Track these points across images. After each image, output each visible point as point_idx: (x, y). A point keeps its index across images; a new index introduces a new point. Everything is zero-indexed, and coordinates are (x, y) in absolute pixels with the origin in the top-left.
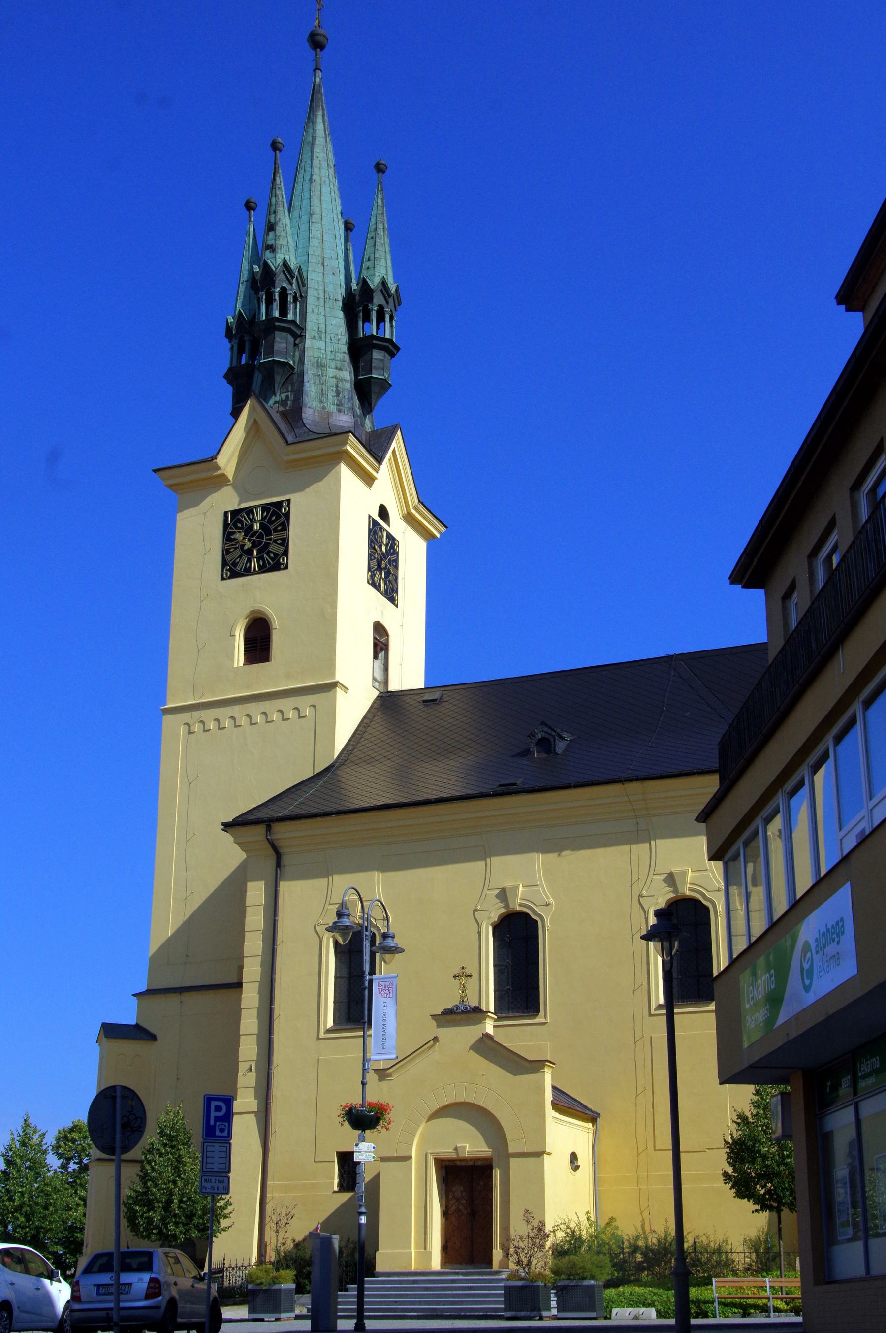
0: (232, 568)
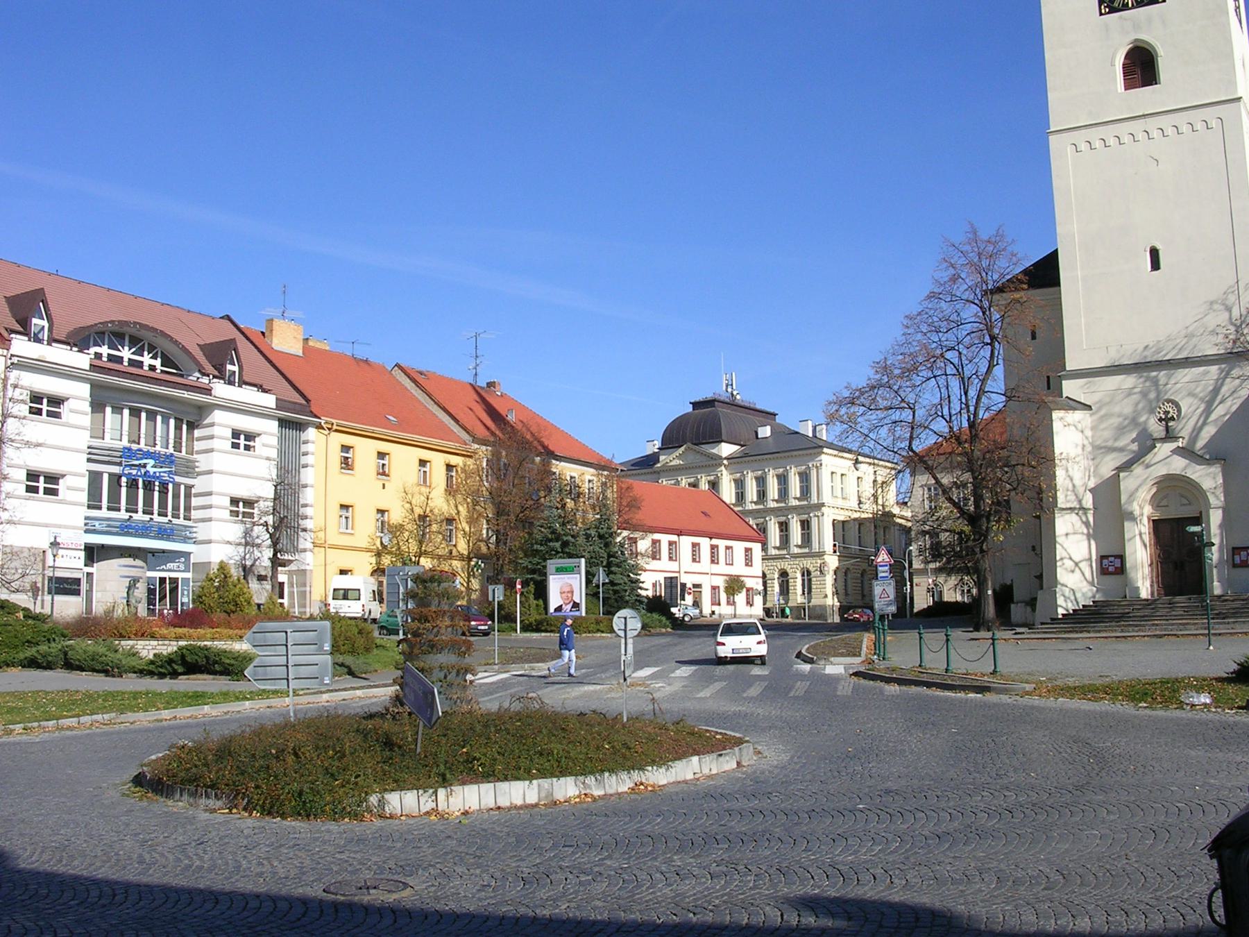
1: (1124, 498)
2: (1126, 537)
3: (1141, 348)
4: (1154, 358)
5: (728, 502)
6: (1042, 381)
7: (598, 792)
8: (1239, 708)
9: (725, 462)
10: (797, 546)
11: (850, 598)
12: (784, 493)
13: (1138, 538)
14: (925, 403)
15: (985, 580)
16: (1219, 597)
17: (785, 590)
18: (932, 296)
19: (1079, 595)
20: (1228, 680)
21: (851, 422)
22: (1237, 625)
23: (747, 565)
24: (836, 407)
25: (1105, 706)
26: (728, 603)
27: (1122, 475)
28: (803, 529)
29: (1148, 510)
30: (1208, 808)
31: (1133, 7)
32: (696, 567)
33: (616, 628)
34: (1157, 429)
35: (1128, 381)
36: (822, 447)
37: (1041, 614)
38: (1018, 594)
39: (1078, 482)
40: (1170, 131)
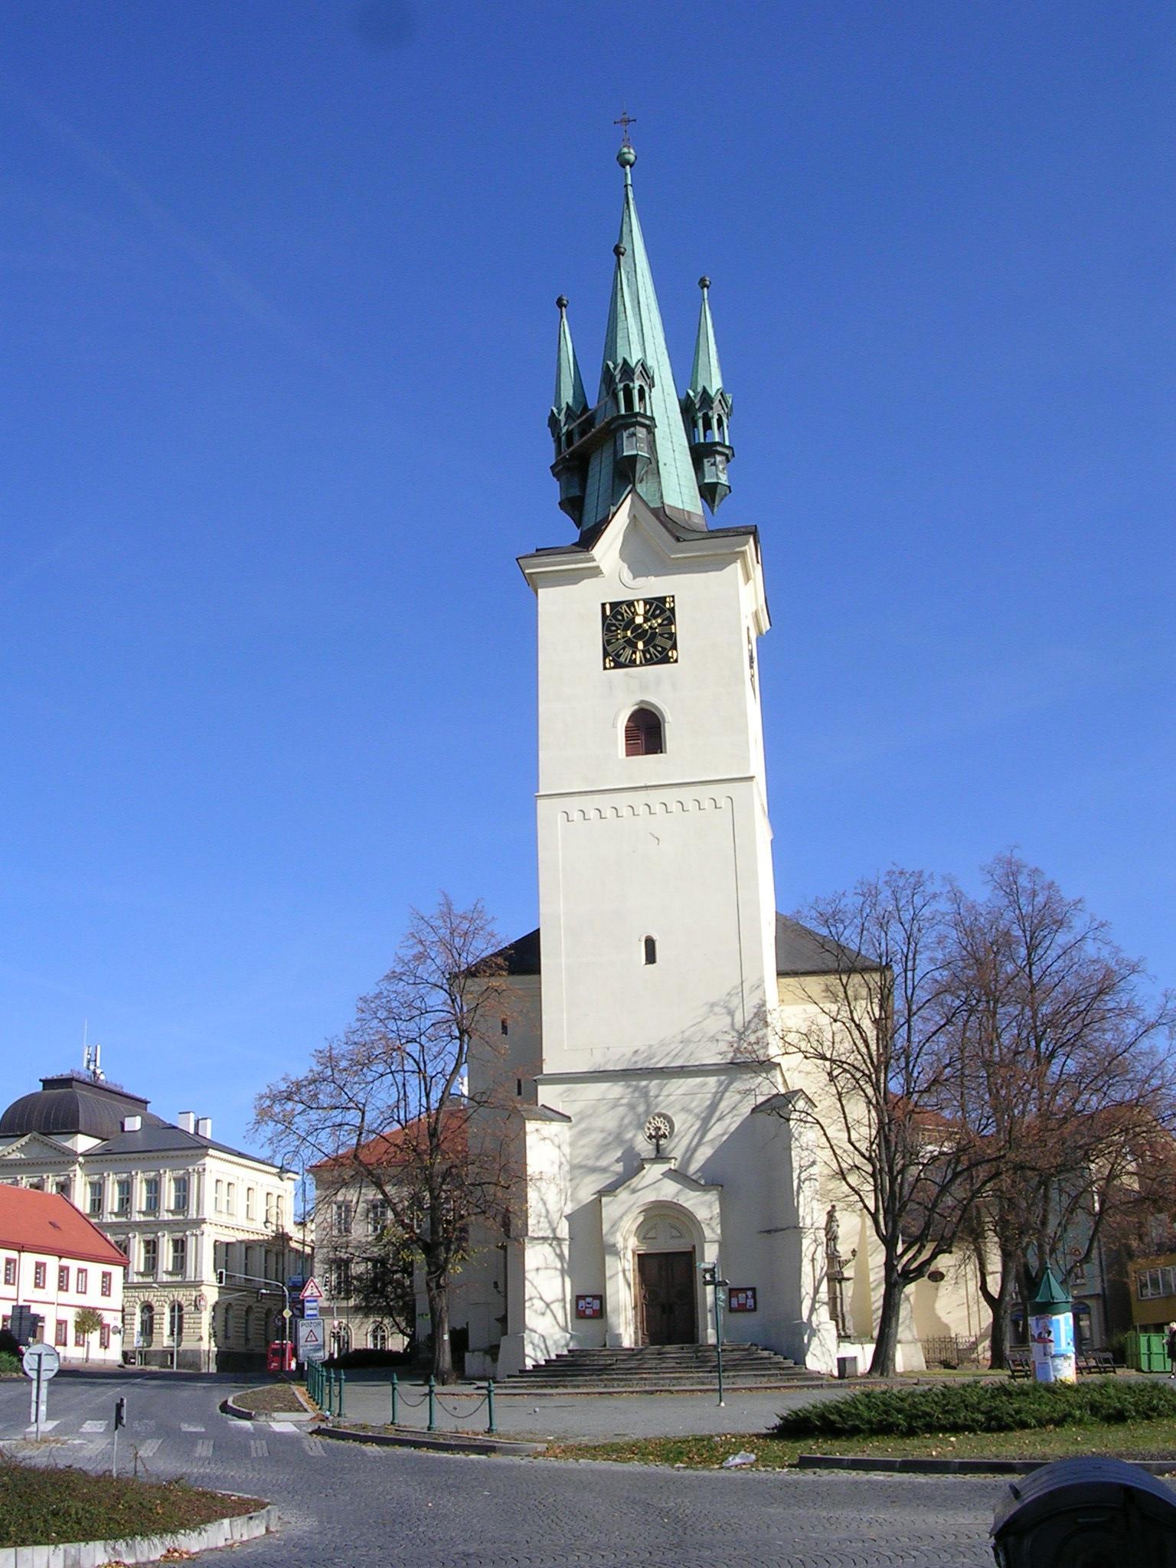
0: (615, 656)
1: (605, 1228)
2: (608, 1274)
3: (629, 1054)
4: (645, 1066)
5: (81, 1209)
6: (515, 1082)
7: (129, 1560)
8: (791, 1466)
9: (81, 1159)
10: (138, 1273)
11: (231, 1342)
12: (154, 1203)
13: (621, 1275)
14: (379, 1104)
15: (441, 1322)
16: (715, 1347)
17: (148, 1329)
18: (394, 977)
19: (549, 1343)
20: (765, 1436)
21: (288, 1122)
22: (738, 1380)
23: (103, 1294)
24: (268, 1102)
25: (635, 1466)
26: (77, 1343)
27: (604, 1199)
28: (176, 1250)
29: (633, 1242)
30: (858, 1560)
31: (641, 665)
32: (39, 1294)
33: (26, 1367)
34: (644, 1146)
35: (615, 1090)
36: (207, 1148)
37: (503, 1366)
38: (474, 1340)
39: (553, 1207)
40: (674, 807)
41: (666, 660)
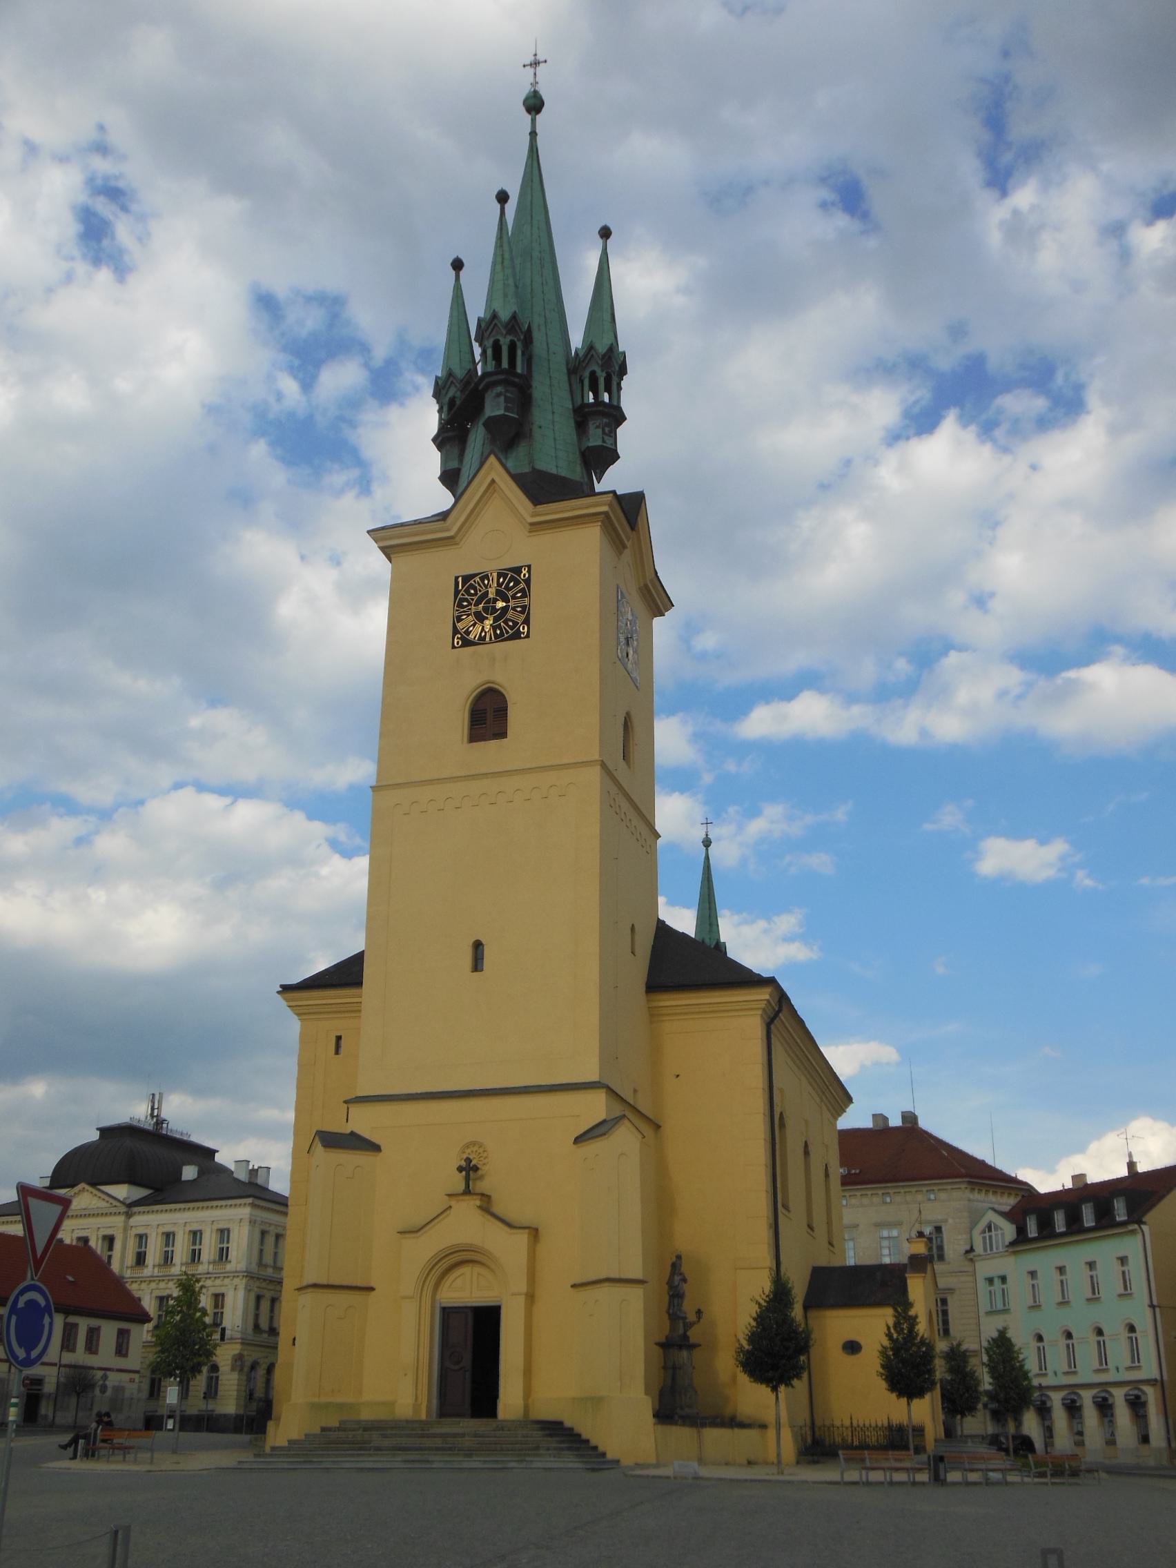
31: (491, 642)
41: (517, 636)
